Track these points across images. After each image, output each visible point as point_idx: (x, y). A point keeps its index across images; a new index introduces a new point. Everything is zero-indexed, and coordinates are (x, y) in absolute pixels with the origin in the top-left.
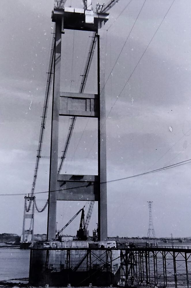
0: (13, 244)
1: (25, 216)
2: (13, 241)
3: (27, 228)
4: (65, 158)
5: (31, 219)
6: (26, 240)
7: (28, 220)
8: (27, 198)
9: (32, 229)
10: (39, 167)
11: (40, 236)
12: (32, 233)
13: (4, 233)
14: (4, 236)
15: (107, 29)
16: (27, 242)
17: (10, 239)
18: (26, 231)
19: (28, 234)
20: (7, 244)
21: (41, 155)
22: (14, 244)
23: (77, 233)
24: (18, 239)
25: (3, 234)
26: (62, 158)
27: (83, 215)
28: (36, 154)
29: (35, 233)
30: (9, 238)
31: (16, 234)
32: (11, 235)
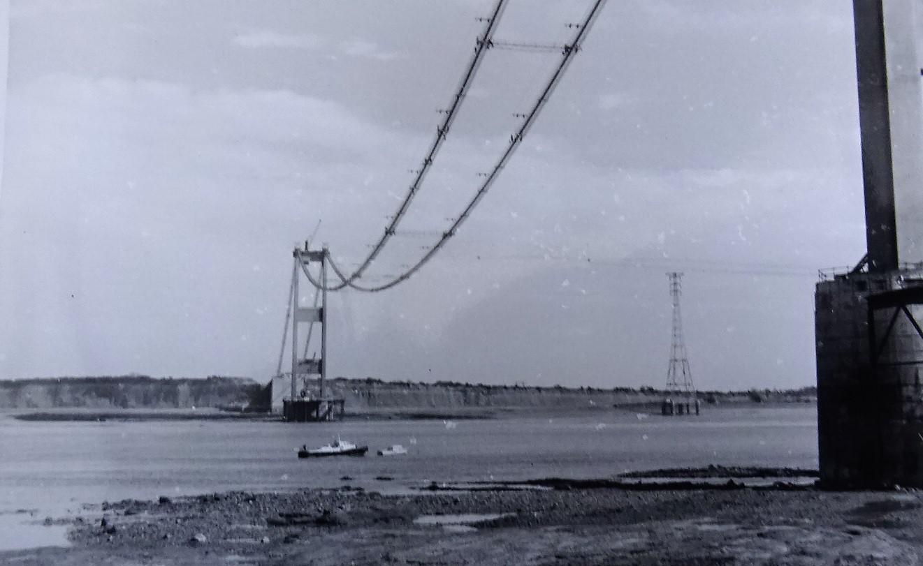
8: (303, 253)
14: (213, 386)
16: (307, 399)
20: (221, 408)
22: (247, 410)
31: (250, 380)
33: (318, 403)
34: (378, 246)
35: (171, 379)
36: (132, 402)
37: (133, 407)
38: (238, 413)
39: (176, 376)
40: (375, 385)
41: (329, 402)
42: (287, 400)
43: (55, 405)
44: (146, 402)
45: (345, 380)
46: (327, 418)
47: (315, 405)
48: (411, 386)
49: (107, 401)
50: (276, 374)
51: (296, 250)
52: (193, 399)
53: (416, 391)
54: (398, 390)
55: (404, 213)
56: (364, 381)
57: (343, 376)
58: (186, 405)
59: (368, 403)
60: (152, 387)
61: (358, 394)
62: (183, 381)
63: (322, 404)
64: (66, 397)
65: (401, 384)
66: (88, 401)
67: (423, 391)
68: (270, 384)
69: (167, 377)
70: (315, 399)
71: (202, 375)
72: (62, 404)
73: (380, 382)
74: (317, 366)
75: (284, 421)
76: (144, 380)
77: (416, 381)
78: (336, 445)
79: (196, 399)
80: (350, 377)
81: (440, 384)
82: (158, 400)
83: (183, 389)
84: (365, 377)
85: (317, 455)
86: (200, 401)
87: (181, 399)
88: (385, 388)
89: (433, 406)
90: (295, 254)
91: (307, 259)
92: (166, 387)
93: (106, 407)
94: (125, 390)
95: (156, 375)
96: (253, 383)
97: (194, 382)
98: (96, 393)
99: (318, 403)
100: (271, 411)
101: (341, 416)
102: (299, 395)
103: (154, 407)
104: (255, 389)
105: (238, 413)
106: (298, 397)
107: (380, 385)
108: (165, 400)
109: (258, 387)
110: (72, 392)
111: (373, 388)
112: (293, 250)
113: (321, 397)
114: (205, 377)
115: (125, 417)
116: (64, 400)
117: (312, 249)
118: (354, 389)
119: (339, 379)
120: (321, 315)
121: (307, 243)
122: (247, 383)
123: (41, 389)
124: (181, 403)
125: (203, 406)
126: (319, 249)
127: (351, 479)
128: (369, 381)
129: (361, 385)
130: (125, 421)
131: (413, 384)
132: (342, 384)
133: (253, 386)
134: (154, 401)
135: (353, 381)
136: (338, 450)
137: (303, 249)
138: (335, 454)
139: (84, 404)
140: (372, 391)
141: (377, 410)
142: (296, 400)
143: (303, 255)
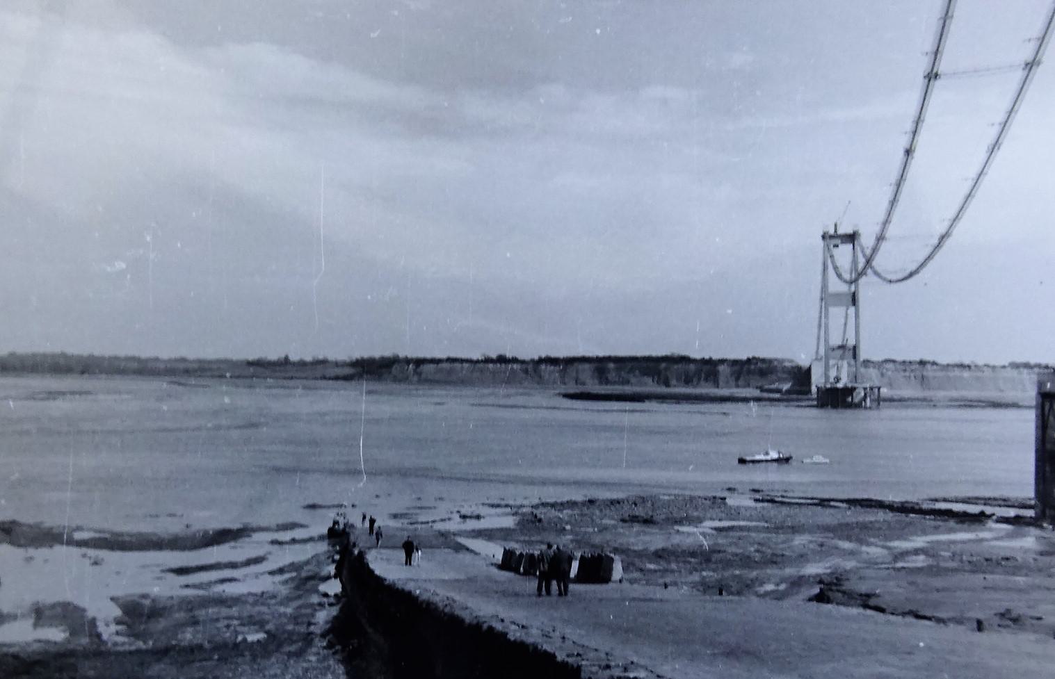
0: (786, 391)
1: (827, 299)
2: (780, 380)
3: (836, 340)
4: (1039, 64)
5: (843, 309)
6: (838, 379)
7: (837, 313)
8: (831, 237)
9: (851, 342)
10: (909, 126)
11: (874, 367)
12: (855, 356)
13: (751, 356)
14: (753, 367)
15: (356, 503)
16: (840, 385)
17: (774, 377)
18: (833, 349)
19: (842, 358)
20: (762, 390)
21: (942, 67)
22: (788, 392)
23: (372, 566)
24: (801, 376)
25: (749, 360)
26: (1029, 66)
27: (838, 367)
28: (923, 65)
29: (863, 355)
30: (772, 373)
31: (791, 361)
32: (776, 363)
33: (853, 389)
34: (954, 220)
35: (711, 359)
36: (674, 382)
37: (675, 386)
38: (777, 396)
39: (716, 356)
40: (929, 366)
41: (865, 389)
42: (819, 386)
43: (601, 383)
44: (688, 381)
45: (894, 361)
46: (863, 404)
47: (849, 391)
48: (973, 368)
49: (650, 380)
50: (814, 358)
51: (825, 233)
52: (733, 378)
53: (979, 374)
54: (957, 372)
55: (890, 201)
56: (916, 362)
57: (893, 357)
58: (727, 385)
59: (922, 385)
60: (692, 367)
61: (910, 377)
62: (722, 361)
63: (857, 391)
64: (612, 376)
65: (962, 366)
66: (633, 380)
67: (988, 373)
68: (810, 366)
69: (707, 357)
70: (850, 385)
71: (743, 356)
72: (607, 382)
73: (934, 363)
74: (851, 352)
75: (817, 406)
76: (684, 360)
77: (981, 362)
78: (767, 454)
79: (737, 379)
80: (899, 358)
81: (1015, 366)
82: (699, 379)
83: (721, 368)
84: (918, 359)
85: (753, 462)
86: (740, 382)
87: (722, 379)
88: (942, 370)
89: (1002, 391)
90: (824, 237)
91: (838, 241)
92: (707, 367)
93: (650, 386)
94: (666, 369)
95: (696, 355)
96: (794, 364)
97: (735, 363)
98: (640, 371)
99: (853, 389)
100: (811, 394)
101: (879, 400)
102: (833, 381)
103: (695, 387)
104: (796, 370)
105: (777, 396)
106: (831, 383)
107: (935, 367)
108: (706, 380)
109: (799, 368)
110: (618, 370)
111: (927, 370)
112: (822, 233)
113: (856, 382)
114: (744, 357)
115: (662, 398)
116: (610, 378)
117: (841, 231)
118: (905, 370)
119: (887, 361)
120: (854, 300)
121: (836, 225)
122: (787, 364)
123: (587, 366)
124: (721, 383)
125: (744, 387)
126: (850, 231)
127: (492, 564)
128: (922, 363)
129: (913, 367)
130: (662, 402)
131: (976, 366)
132: (890, 366)
133: (792, 368)
134: (695, 380)
135: (904, 362)
136: (769, 458)
137: (832, 232)
138: (767, 461)
139: (628, 382)
140: (925, 373)
141: (927, 394)
142: (828, 386)
143: (832, 238)
